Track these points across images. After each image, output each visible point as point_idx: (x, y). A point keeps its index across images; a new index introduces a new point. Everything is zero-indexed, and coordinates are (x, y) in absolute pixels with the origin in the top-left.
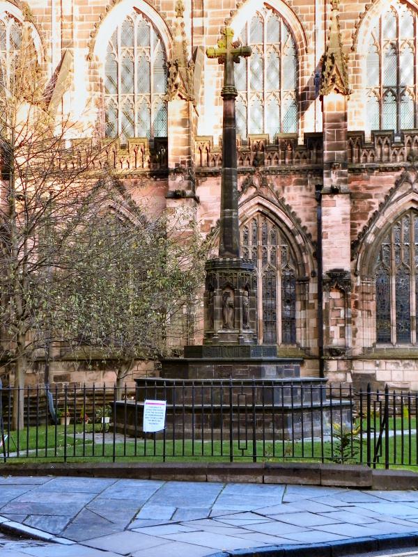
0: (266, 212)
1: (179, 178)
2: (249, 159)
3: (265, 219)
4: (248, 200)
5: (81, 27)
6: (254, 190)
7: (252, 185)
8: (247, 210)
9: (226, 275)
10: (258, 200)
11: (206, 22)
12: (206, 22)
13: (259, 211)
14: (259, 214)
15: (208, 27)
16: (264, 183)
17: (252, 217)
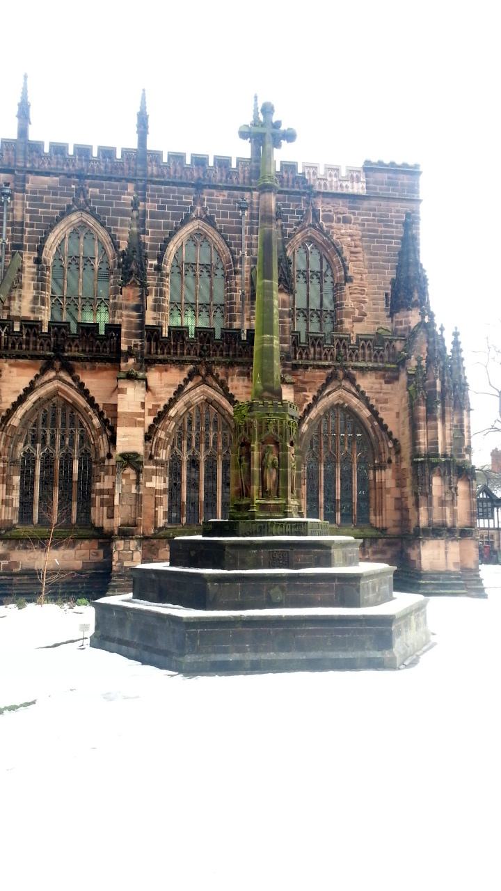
5: (30, 233)
6: (200, 378)
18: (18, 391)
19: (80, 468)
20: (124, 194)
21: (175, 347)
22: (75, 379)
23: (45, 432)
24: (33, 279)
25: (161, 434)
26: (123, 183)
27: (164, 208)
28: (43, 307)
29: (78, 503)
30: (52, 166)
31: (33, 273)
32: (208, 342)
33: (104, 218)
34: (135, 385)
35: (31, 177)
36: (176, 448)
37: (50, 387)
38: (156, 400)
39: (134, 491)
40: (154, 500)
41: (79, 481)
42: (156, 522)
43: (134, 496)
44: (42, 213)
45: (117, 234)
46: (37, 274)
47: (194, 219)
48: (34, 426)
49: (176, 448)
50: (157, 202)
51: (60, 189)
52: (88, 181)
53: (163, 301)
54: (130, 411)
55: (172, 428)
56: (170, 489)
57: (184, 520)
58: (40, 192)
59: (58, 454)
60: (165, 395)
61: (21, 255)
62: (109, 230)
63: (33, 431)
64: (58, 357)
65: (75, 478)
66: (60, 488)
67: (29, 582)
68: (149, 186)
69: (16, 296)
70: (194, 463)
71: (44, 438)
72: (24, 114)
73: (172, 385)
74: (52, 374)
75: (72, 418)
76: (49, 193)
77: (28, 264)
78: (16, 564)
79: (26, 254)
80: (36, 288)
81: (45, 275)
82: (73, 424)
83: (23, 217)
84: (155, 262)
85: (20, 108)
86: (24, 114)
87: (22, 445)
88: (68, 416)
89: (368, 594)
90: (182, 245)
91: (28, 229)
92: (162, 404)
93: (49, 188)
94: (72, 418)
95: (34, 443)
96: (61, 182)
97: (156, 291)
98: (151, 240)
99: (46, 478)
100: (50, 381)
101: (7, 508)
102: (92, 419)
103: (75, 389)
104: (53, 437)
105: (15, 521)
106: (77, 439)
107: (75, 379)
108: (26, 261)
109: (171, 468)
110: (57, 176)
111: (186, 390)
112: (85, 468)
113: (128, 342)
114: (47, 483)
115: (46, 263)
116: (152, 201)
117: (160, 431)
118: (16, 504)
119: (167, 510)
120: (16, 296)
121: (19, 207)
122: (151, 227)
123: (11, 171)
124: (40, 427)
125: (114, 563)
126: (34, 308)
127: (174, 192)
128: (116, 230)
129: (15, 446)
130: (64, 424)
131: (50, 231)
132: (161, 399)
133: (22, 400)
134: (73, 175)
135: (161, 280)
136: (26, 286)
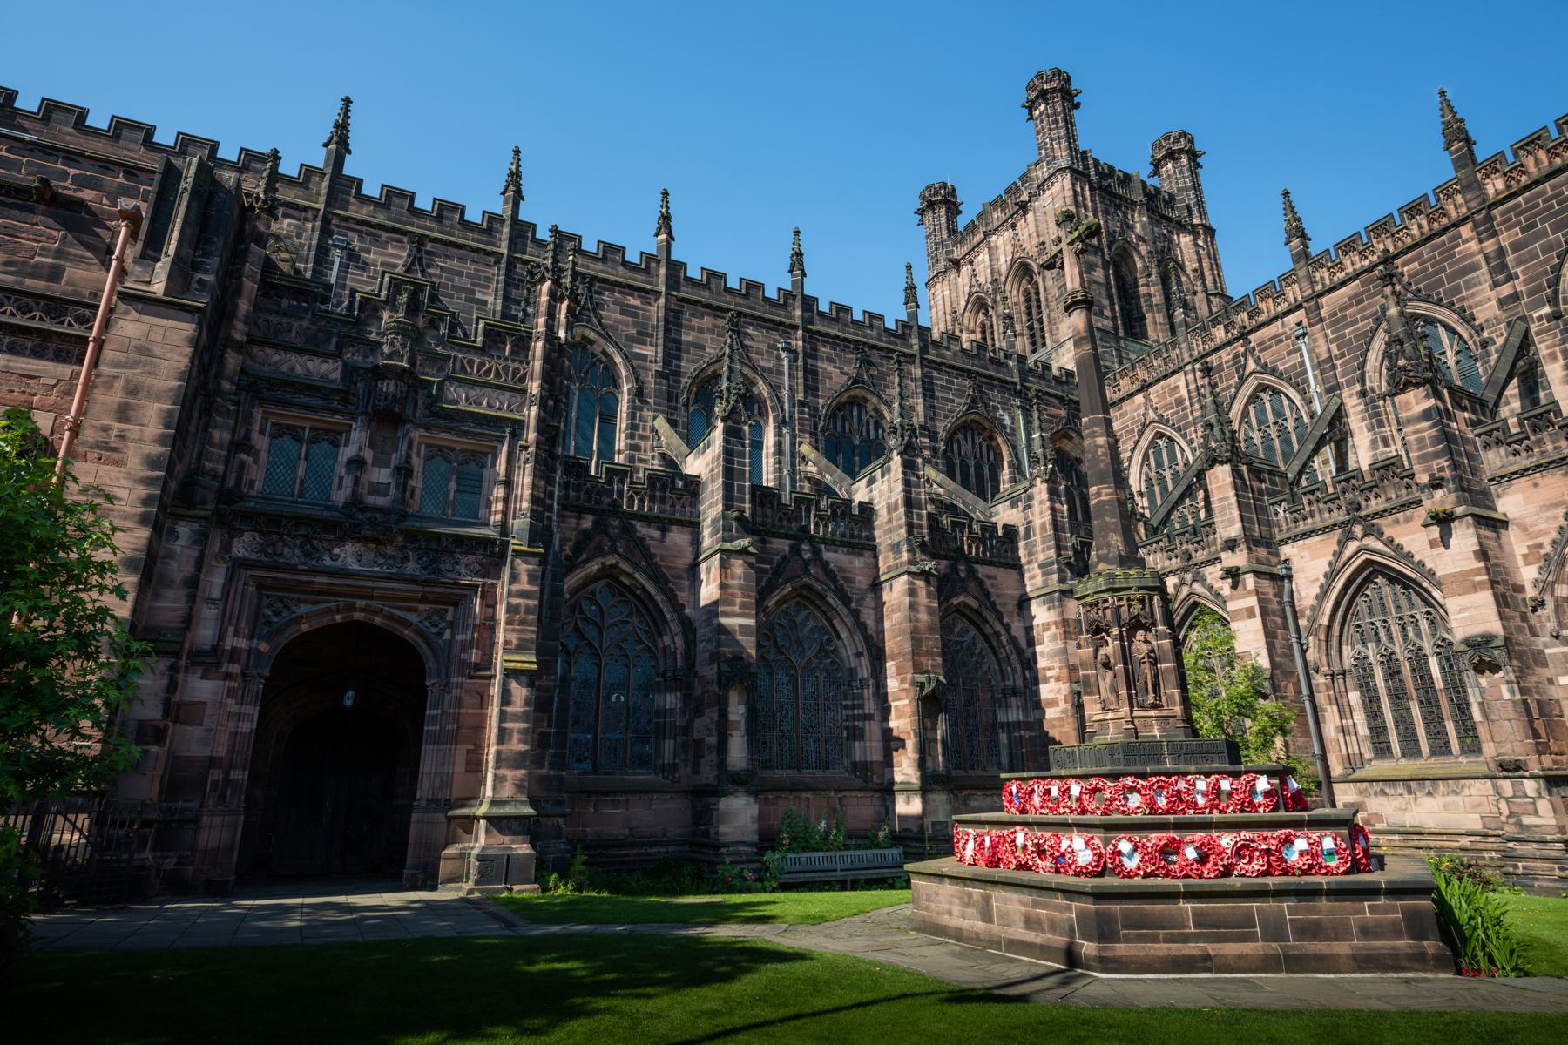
5: (1342, 365)
18: (1317, 580)
20: (1458, 245)
24: (1363, 419)
26: (1452, 233)
45: (1466, 304)
46: (1367, 410)
51: (1363, 292)
52: (1398, 261)
54: (1458, 570)
58: (1340, 310)
65: (1439, 685)
67: (1402, 844)
68: (1495, 212)
76: (1352, 305)
78: (1379, 817)
79: (1345, 393)
80: (1371, 429)
83: (1329, 350)
84: (1547, 310)
86: (1297, 232)
91: (1338, 362)
96: (1363, 285)
98: (1526, 282)
112: (1451, 667)
114: (1398, 696)
118: (1363, 730)
121: (1321, 342)
122: (1518, 265)
127: (1544, 192)
130: (1398, 608)
131: (1368, 350)
132: (1542, 533)
133: (1325, 591)
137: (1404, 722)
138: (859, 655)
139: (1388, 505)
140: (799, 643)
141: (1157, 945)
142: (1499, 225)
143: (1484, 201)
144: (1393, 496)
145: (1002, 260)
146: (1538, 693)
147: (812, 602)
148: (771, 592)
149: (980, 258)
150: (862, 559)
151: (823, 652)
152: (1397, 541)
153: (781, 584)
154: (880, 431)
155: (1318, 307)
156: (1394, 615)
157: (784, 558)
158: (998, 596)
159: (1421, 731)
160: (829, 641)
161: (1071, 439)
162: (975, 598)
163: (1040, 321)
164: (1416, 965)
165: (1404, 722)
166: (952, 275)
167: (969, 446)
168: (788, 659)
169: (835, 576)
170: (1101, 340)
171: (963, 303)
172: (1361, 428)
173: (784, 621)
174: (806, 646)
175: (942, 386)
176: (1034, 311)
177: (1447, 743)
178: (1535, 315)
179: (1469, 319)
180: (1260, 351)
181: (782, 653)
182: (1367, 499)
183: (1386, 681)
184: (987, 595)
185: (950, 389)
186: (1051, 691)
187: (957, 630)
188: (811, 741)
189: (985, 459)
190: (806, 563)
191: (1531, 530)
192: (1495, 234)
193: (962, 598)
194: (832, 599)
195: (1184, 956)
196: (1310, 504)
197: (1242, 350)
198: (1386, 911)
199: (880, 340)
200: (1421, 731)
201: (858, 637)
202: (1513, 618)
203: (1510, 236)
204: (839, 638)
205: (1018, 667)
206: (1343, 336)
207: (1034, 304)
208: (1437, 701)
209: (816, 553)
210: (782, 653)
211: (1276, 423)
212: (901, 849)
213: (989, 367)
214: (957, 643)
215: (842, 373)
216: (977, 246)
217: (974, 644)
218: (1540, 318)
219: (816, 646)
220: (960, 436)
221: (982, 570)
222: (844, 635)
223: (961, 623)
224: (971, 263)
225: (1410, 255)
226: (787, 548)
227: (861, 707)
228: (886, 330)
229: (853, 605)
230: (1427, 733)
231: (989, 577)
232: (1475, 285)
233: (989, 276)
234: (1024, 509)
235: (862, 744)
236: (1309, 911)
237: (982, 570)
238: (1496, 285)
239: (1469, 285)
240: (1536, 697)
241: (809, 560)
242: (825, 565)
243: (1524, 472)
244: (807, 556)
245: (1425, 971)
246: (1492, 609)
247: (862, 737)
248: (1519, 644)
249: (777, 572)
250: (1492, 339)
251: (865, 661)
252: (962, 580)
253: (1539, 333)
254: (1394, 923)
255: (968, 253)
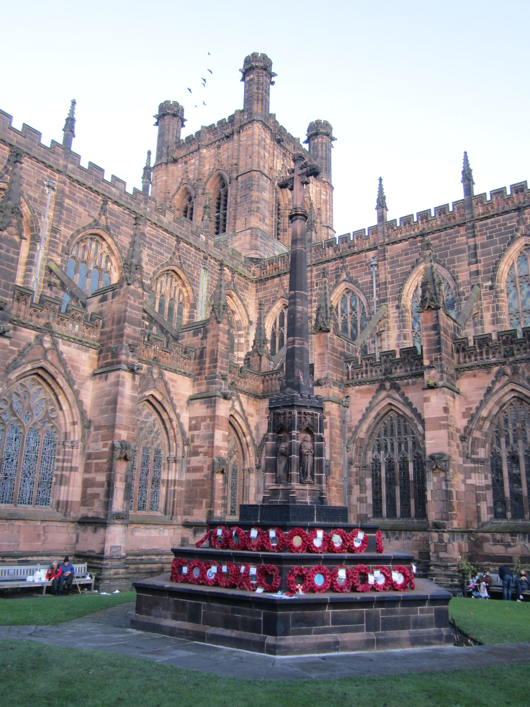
0: (522, 396)
1: (433, 372)
2: (500, 352)
3: (522, 404)
4: (502, 388)
5: (391, 288)
6: (506, 378)
7: (505, 374)
8: (503, 396)
9: (279, 414)
10: (511, 386)
11: (480, 267)
12: (480, 267)
13: (515, 397)
14: (516, 399)
15: (481, 269)
16: (515, 372)
17: (509, 403)
18: (362, 411)
19: (414, 469)
20: (458, 237)
21: (481, 353)
22: (403, 395)
23: (386, 440)
24: (396, 322)
25: (477, 434)
27: (492, 237)
28: (405, 341)
29: (416, 500)
30: (403, 234)
31: (396, 317)
32: (512, 342)
33: (444, 261)
34: (437, 393)
35: (389, 247)
36: (494, 446)
37: (384, 404)
38: (469, 404)
39: (444, 487)
40: (474, 497)
41: (414, 481)
42: (479, 518)
43: (444, 492)
44: (399, 271)
45: (456, 270)
46: (399, 317)
47: (519, 237)
48: (379, 437)
49: (494, 446)
50: (486, 234)
51: (410, 249)
53: (500, 314)
54: (434, 416)
55: (487, 428)
56: (494, 485)
57: (509, 514)
58: (396, 256)
59: (396, 458)
60: (477, 397)
61: (387, 306)
62: (448, 269)
63: (378, 440)
64: (388, 379)
65: (411, 478)
66: (401, 487)
69: (386, 337)
70: (514, 459)
71: (386, 446)
72: (381, 204)
73: (481, 388)
74: (383, 394)
75: (405, 427)
77: (393, 312)
80: (399, 328)
81: (405, 317)
82: (406, 432)
84: (489, 283)
85: (463, 175)
86: (381, 204)
87: (371, 452)
88: (402, 427)
89: (307, 502)
90: (513, 263)
91: (390, 286)
92: (474, 406)
93: (402, 251)
94: (405, 427)
95: (379, 450)
96: (411, 244)
97: (493, 307)
98: (484, 266)
99: (390, 479)
100: (384, 399)
101: (362, 504)
102: (417, 426)
103: (402, 403)
104: (392, 445)
105: (370, 515)
106: (410, 444)
107: (403, 395)
108: (390, 309)
109: (492, 466)
110: (452, 228)
111: (494, 390)
112: (419, 469)
113: (429, 358)
114: (390, 483)
115: (404, 307)
116: (481, 235)
117: (475, 431)
118: (370, 501)
119: (492, 505)
120: (386, 337)
122: (483, 255)
123: (376, 248)
124: (383, 438)
125: (431, 554)
126: (398, 343)
127: (498, 221)
128: (454, 267)
129: (365, 454)
130: (399, 433)
132: (473, 402)
133: (364, 417)
134: (418, 236)
135: (496, 297)
136: (392, 328)
137: (391, 498)
138: (74, 423)
139: (405, 374)
140: (30, 409)
141: (310, 636)
142: (478, 232)
143: (472, 217)
144: (409, 369)
145: (207, 167)
146: (457, 487)
147: (45, 380)
148: (15, 369)
149: (193, 161)
150: (87, 354)
151: (48, 418)
152: (406, 395)
153: (24, 364)
154: (109, 264)
155: (384, 251)
156: (397, 436)
157: (30, 345)
158: (176, 394)
159: (398, 504)
160: (53, 410)
161: (231, 297)
162: (161, 393)
163: (225, 215)
164: (437, 642)
165: (391, 498)
166: (172, 167)
167: (168, 288)
168: (19, 420)
169: (66, 364)
170: (261, 237)
171: (175, 187)
172: (394, 326)
173: (21, 392)
174: (35, 412)
175: (157, 243)
176: (222, 207)
177: (409, 511)
178: (485, 285)
179: (455, 279)
180: (351, 269)
181: (15, 415)
182: (396, 368)
183: (386, 474)
184: (169, 392)
185: (162, 246)
186: (200, 462)
187: (144, 413)
188: (28, 483)
189: (177, 299)
190: (46, 351)
191: (469, 400)
192: (474, 236)
193: (152, 392)
194: (60, 380)
195: (325, 642)
196: (366, 365)
197: (341, 265)
198: (429, 611)
199: (121, 199)
200: (398, 504)
201: (76, 411)
202: (453, 446)
203: (481, 239)
204: (61, 409)
205: (180, 443)
206: (395, 271)
207: (222, 202)
208: (409, 487)
209: (55, 344)
210: (15, 415)
211: (351, 313)
212: (85, 565)
213: (191, 237)
214: (143, 422)
215: (89, 215)
216: (192, 153)
217: (154, 425)
218: (486, 287)
219: (42, 413)
220: (163, 279)
221: (168, 375)
222: (65, 407)
223: (148, 409)
224: (186, 163)
225: (435, 235)
226: (33, 338)
227: (71, 461)
228: (126, 193)
229: (76, 387)
230: (401, 504)
231: (172, 380)
232: (462, 261)
233: (197, 175)
234: (202, 339)
235: (66, 488)
236: (391, 613)
237: (168, 375)
238: (469, 264)
239: (459, 260)
240: (457, 489)
241: (49, 349)
242: (59, 355)
243: (469, 368)
244: (47, 345)
245: (440, 644)
246: (446, 440)
247: (67, 483)
248: (454, 460)
249: (22, 354)
250: (464, 292)
251: (78, 428)
252: (155, 380)
253: (484, 295)
254: (430, 618)
255: (185, 156)
